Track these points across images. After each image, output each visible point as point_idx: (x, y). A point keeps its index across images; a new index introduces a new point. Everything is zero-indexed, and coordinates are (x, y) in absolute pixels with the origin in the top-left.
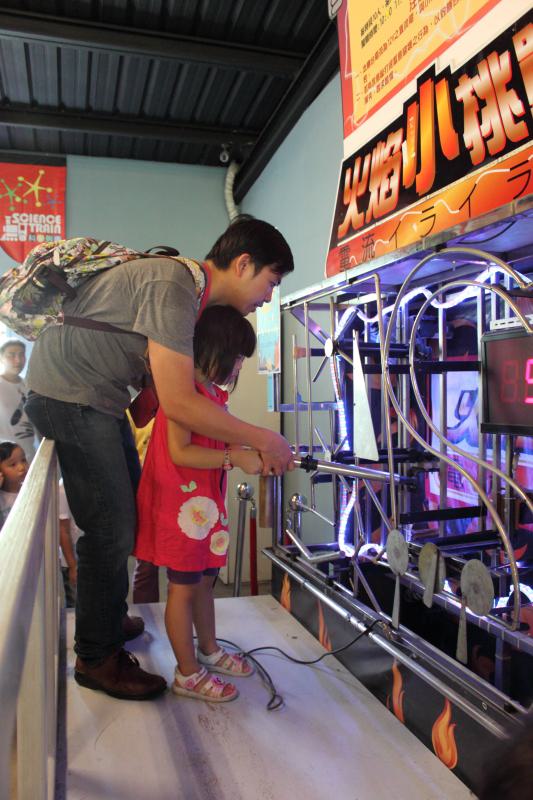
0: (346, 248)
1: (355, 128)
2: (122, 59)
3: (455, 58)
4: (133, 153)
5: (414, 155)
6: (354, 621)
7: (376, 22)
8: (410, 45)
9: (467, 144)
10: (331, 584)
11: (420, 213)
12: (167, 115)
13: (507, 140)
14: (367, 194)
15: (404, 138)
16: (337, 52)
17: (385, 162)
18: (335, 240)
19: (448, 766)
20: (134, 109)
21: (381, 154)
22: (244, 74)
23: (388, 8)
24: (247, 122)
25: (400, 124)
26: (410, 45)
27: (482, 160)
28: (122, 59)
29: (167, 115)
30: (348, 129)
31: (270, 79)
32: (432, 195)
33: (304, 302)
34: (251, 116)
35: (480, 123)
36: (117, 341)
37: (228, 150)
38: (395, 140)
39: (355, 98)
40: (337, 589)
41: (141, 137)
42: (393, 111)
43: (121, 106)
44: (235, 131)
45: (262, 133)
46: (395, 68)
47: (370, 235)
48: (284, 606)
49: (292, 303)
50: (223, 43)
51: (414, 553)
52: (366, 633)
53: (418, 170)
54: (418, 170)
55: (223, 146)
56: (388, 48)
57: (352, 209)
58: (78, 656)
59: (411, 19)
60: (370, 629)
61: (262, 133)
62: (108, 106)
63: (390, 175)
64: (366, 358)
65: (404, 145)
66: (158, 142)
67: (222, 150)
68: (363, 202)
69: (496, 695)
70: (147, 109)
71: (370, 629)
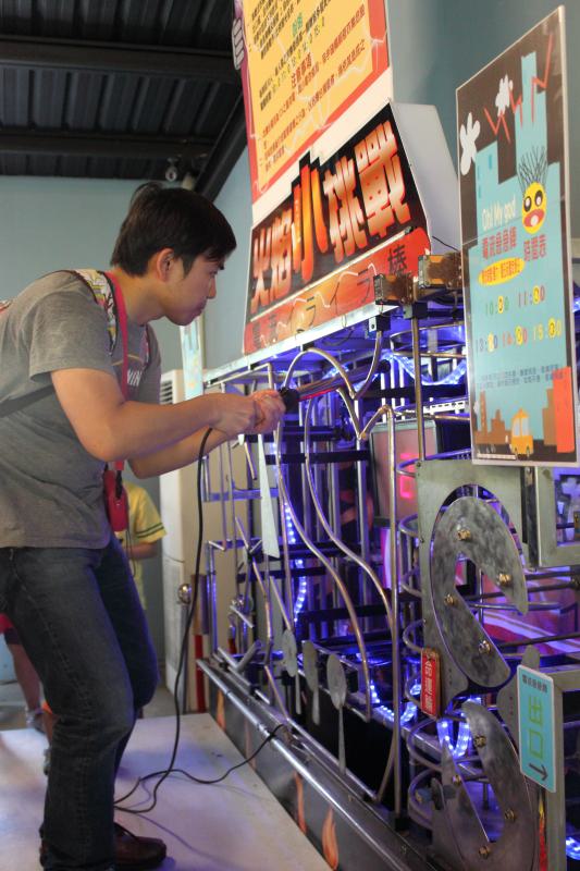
0: (257, 323)
1: (260, 195)
2: (32, 74)
3: (323, 150)
4: (58, 170)
5: (299, 240)
6: (262, 728)
7: (270, 88)
8: (294, 124)
9: (333, 241)
10: (252, 693)
11: (305, 301)
12: (97, 126)
13: (356, 247)
14: (270, 269)
15: (293, 220)
16: (242, 100)
17: (281, 241)
18: (250, 315)
19: (332, 867)
20: (55, 122)
21: (277, 231)
22: (183, 82)
23: (308, 51)
24: (199, 129)
25: (288, 204)
26: (294, 124)
27: (287, 292)
28: (32, 74)
29: (97, 126)
30: (255, 196)
31: (217, 86)
32: (312, 286)
33: (221, 382)
34: (201, 121)
35: (339, 223)
36: (26, 425)
37: (177, 165)
38: (287, 219)
39: (259, 163)
40: (258, 698)
41: (65, 155)
42: (282, 190)
43: (38, 118)
44: (185, 141)
45: (218, 141)
46: (285, 142)
47: (273, 316)
48: (220, 725)
49: (253, 366)
50: (155, 48)
51: (322, 663)
52: (269, 739)
53: (303, 257)
54: (303, 257)
55: (170, 160)
56: (281, 119)
57: (260, 284)
58: (44, 843)
59: (293, 97)
60: (273, 735)
61: (218, 141)
62: (20, 119)
63: (285, 255)
64: (315, 444)
65: (293, 227)
66: (89, 159)
67: (169, 165)
68: (267, 279)
69: (354, 782)
70: (70, 120)
71: (273, 735)
